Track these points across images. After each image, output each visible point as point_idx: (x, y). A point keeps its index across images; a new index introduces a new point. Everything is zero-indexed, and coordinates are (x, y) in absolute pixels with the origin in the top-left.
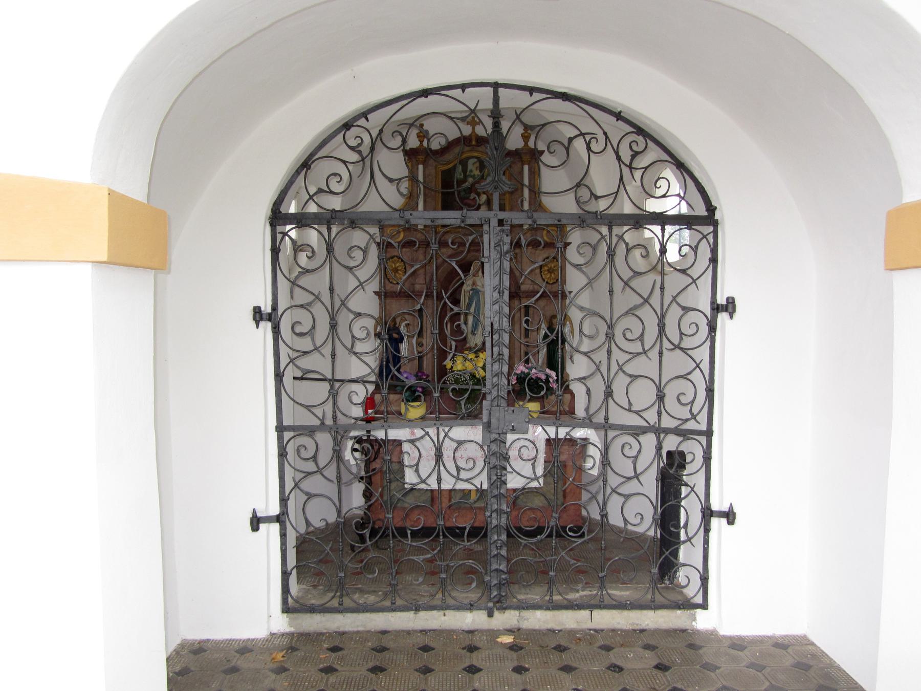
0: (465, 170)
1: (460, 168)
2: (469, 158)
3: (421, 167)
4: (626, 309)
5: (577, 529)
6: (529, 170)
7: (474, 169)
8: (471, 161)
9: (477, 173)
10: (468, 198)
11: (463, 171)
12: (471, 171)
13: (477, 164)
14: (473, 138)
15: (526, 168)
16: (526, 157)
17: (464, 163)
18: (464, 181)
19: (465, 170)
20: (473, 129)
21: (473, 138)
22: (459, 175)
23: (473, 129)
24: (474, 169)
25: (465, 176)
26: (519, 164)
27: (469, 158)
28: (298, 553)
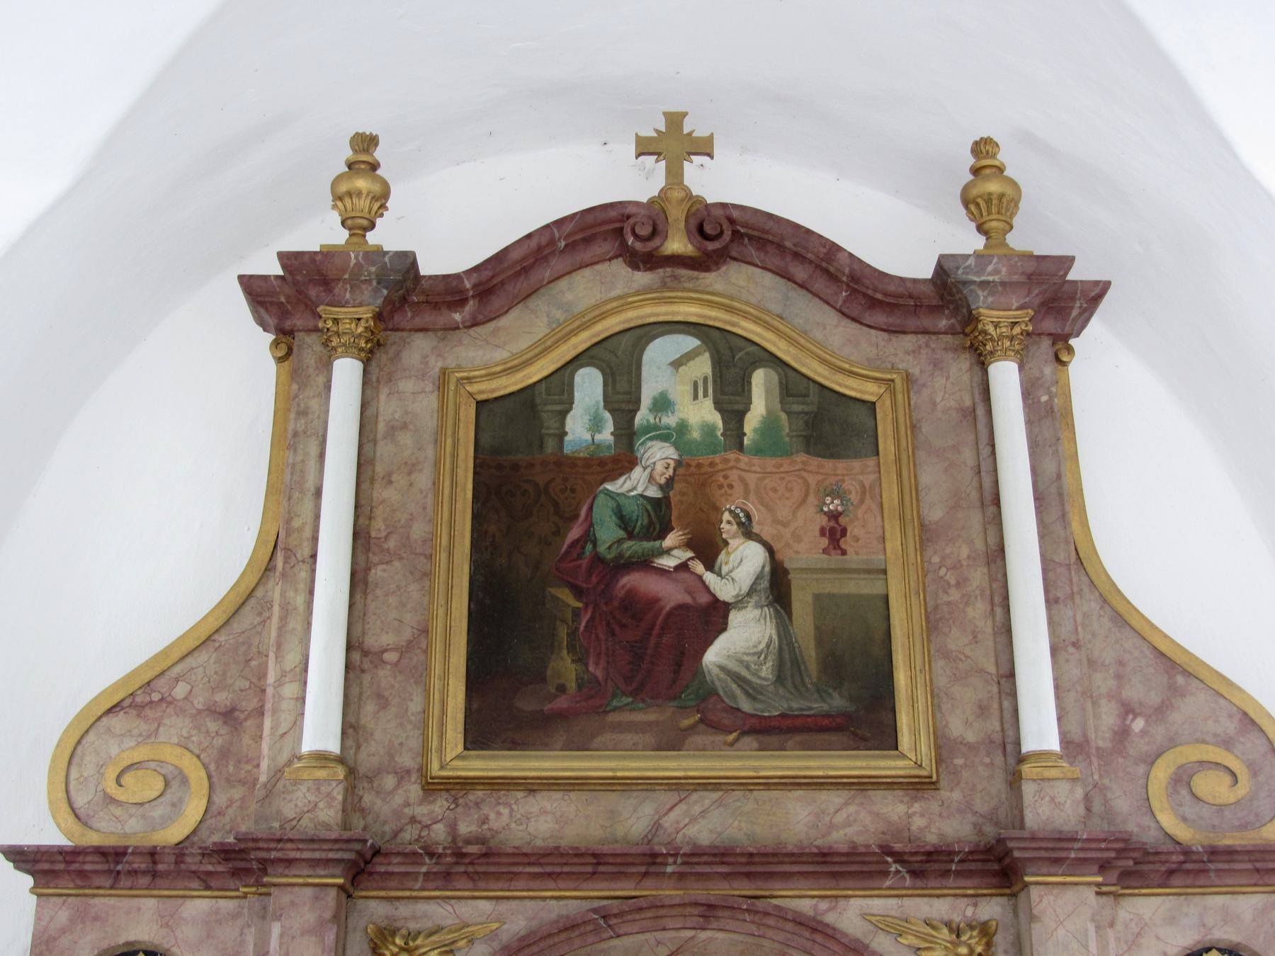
0: (622, 399)
1: (589, 386)
2: (647, 332)
3: (346, 374)
4: (108, 706)
5: (707, 622)
6: (1028, 393)
7: (680, 392)
8: (660, 352)
9: (701, 414)
10: (644, 564)
11: (609, 402)
12: (663, 404)
13: (703, 366)
14: (677, 215)
15: (1006, 377)
16: (996, 316)
17: (619, 359)
18: (623, 461)
19: (622, 399)
20: (675, 174)
21: (677, 215)
22: (584, 423)
23: (675, 174)
24: (680, 392)
25: (627, 434)
26: (960, 367)
27: (647, 332)
28: (1051, 601)
